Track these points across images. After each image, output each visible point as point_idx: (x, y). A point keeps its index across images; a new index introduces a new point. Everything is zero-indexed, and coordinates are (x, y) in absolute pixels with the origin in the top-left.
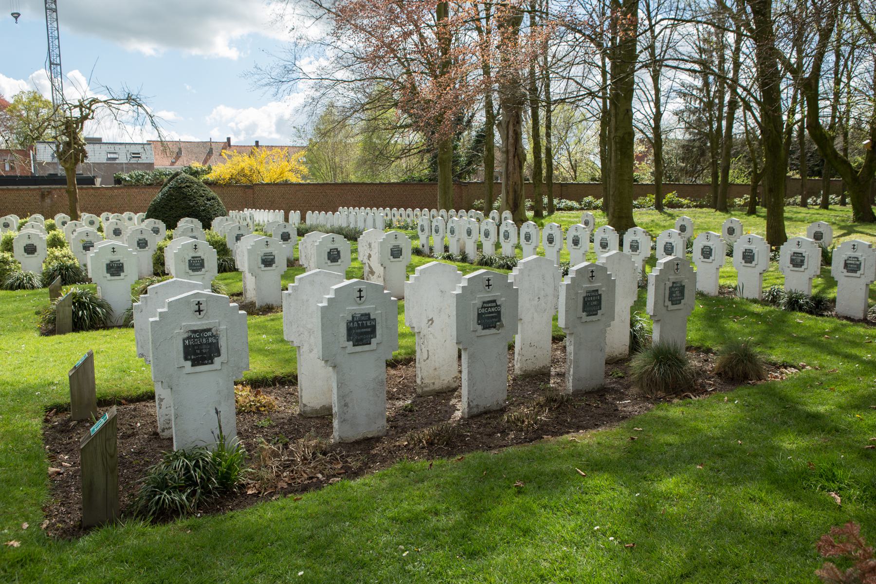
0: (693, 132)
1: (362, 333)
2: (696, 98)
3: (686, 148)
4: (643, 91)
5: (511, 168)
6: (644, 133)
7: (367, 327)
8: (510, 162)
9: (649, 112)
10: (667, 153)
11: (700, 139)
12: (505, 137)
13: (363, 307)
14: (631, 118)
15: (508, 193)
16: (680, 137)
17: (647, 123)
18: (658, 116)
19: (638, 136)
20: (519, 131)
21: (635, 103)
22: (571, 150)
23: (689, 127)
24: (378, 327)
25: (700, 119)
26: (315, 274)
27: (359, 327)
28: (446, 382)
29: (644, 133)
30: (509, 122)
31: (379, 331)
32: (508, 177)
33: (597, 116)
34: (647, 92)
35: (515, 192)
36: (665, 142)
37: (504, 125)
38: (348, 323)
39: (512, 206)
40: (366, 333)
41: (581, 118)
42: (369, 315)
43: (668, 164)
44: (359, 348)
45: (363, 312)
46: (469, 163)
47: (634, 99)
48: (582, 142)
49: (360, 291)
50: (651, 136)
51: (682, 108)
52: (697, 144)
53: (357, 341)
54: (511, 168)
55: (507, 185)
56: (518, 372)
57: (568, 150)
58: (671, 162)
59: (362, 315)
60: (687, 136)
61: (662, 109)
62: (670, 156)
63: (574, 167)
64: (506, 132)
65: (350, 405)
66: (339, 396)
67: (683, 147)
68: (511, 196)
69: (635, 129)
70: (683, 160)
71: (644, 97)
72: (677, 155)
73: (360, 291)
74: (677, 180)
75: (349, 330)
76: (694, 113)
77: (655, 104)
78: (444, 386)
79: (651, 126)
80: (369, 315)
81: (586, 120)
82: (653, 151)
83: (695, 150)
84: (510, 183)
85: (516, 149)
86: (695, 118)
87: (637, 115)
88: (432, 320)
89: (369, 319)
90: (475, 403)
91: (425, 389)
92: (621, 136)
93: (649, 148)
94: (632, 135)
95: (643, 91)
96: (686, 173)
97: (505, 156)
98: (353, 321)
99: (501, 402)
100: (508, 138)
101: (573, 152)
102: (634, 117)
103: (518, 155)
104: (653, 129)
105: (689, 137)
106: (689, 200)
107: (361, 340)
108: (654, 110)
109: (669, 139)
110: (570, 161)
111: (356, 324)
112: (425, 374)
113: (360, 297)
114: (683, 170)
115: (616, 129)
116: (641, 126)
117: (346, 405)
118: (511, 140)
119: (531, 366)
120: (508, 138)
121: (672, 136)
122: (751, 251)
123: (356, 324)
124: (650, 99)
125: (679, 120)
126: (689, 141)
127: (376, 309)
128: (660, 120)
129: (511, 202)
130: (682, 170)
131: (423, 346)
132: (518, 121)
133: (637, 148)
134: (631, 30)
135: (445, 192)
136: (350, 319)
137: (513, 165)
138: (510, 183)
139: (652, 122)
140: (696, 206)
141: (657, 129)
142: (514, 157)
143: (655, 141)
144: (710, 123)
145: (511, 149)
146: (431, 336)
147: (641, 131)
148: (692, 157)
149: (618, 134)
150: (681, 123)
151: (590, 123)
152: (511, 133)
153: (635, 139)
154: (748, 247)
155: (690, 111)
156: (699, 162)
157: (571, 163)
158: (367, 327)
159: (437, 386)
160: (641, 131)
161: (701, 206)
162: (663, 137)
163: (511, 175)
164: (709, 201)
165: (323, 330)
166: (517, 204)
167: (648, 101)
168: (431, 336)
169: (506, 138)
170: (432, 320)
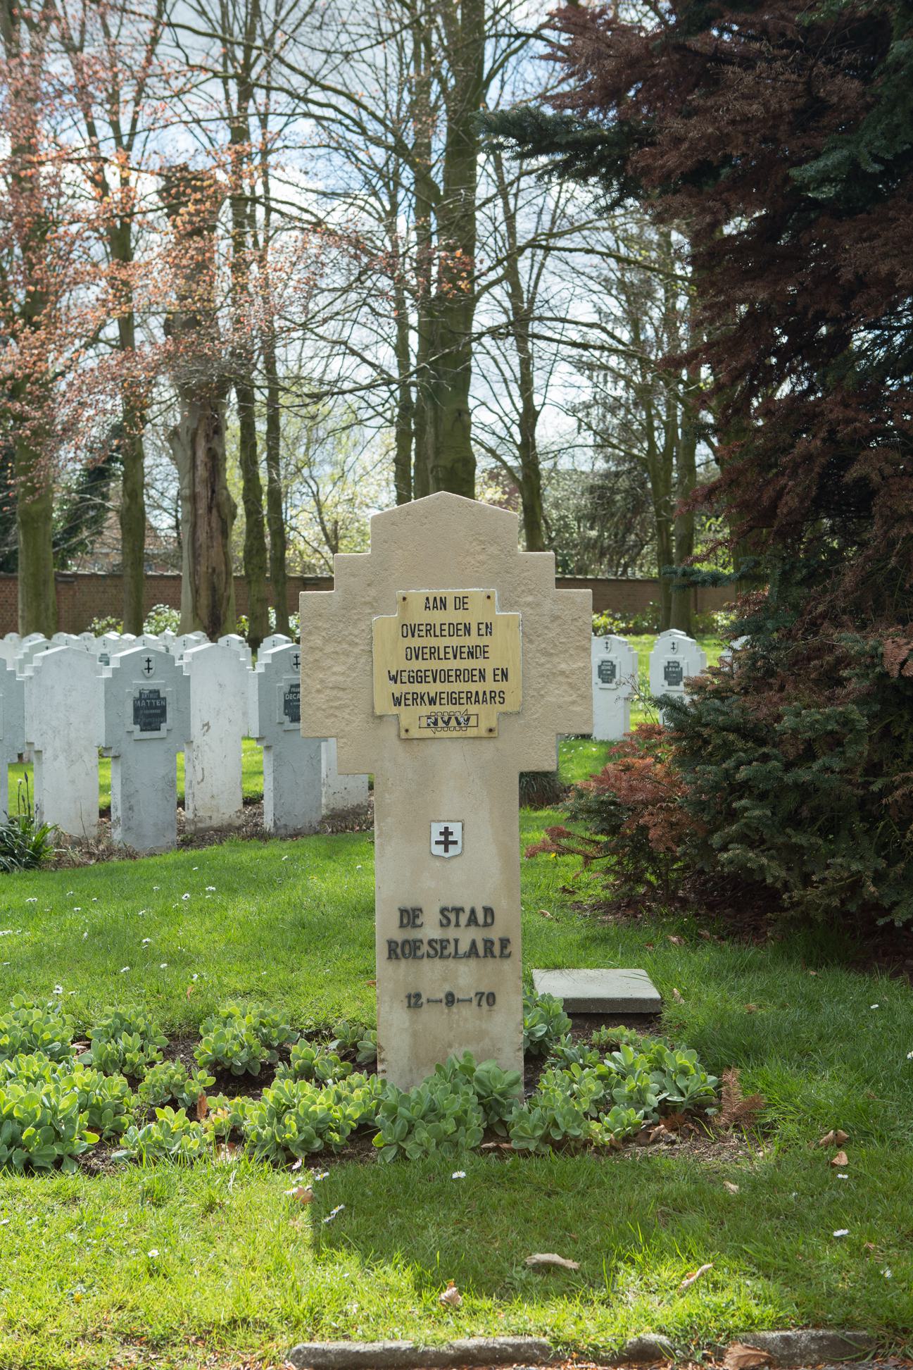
0: (613, 454)
1: (150, 716)
2: (618, 376)
3: (601, 492)
4: (493, 358)
5: (202, 536)
6: (498, 458)
7: (156, 707)
8: (200, 522)
9: (508, 407)
10: (556, 506)
11: (629, 471)
12: (188, 464)
13: (151, 682)
14: (467, 427)
15: (196, 592)
16: (586, 468)
17: (503, 433)
18: (529, 418)
19: (484, 463)
20: (220, 451)
21: (477, 389)
22: (322, 498)
23: (603, 443)
24: (169, 709)
25: (625, 426)
26: (62, 651)
27: (148, 708)
28: (227, 816)
29: (498, 458)
30: (197, 429)
31: (169, 715)
32: (195, 556)
33: (388, 415)
34: (501, 360)
35: (213, 589)
36: (550, 478)
37: (185, 438)
38: (136, 700)
39: (206, 621)
40: (156, 715)
41: (349, 418)
42: (158, 692)
43: (558, 531)
44: (147, 735)
45: (151, 688)
46: (72, 531)
47: (473, 377)
48: (350, 477)
49: (148, 661)
50: (513, 462)
51: (586, 396)
52: (623, 483)
53: (145, 724)
54: (202, 536)
55: (194, 573)
56: (324, 812)
57: (316, 496)
58: (567, 526)
59: (151, 692)
60: (601, 465)
61: (537, 400)
62: (564, 512)
63: (332, 539)
64: (189, 453)
65: (135, 808)
66: (123, 795)
67: (592, 489)
68: (204, 600)
69: (475, 448)
70: (593, 519)
71: (497, 371)
72: (578, 508)
73: (148, 661)
74: (582, 569)
75: (137, 709)
76: (613, 410)
77: (520, 387)
78: (225, 823)
79: (514, 442)
80: (158, 692)
81: (360, 422)
82: (520, 500)
83: (618, 497)
84: (202, 569)
85: (213, 492)
86: (616, 421)
87: (480, 416)
88: (207, 724)
89: (159, 697)
90: (283, 822)
91: (200, 825)
92: (449, 465)
93: (511, 494)
94: (470, 463)
95: (493, 358)
96: (602, 555)
97: (189, 506)
98: (140, 699)
99: (315, 824)
100: (194, 466)
101: (329, 502)
102: (473, 419)
103: (218, 506)
104: (519, 447)
105: (605, 466)
106: (609, 615)
107: (150, 724)
108: (520, 405)
109: (558, 472)
110: (322, 522)
111: (143, 704)
112: (199, 803)
113: (149, 669)
114: (594, 547)
115: (437, 452)
116: (491, 441)
117: (131, 808)
118: (202, 472)
119: (340, 804)
120: (194, 466)
121: (565, 463)
122: (676, 664)
123: (143, 704)
124: (508, 374)
125: (580, 427)
126: (607, 475)
127: (165, 685)
128: (534, 425)
129: (204, 613)
130: (589, 545)
131: (196, 762)
132: (217, 430)
133: (483, 493)
134: (463, 279)
135: (37, 594)
136: (137, 695)
137: (206, 528)
138: (202, 569)
139: (515, 430)
140: (625, 632)
141: (527, 447)
142: (210, 509)
143: (526, 476)
144: (648, 431)
145: (202, 490)
146: (206, 748)
147: (491, 451)
148: (613, 515)
149: (441, 463)
150: (584, 434)
151: (369, 433)
152: (201, 454)
153: (477, 472)
154: (672, 657)
155: (604, 405)
156: (629, 529)
157: (324, 529)
158: (156, 707)
159: (215, 822)
160: (491, 451)
161: (637, 631)
162: (545, 465)
163: (204, 552)
164: (655, 620)
165: (106, 708)
166: (218, 618)
167: (505, 381)
168: (206, 748)
169: (188, 469)
170: (207, 724)
